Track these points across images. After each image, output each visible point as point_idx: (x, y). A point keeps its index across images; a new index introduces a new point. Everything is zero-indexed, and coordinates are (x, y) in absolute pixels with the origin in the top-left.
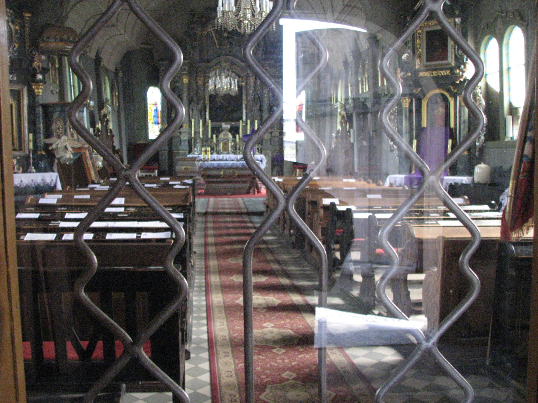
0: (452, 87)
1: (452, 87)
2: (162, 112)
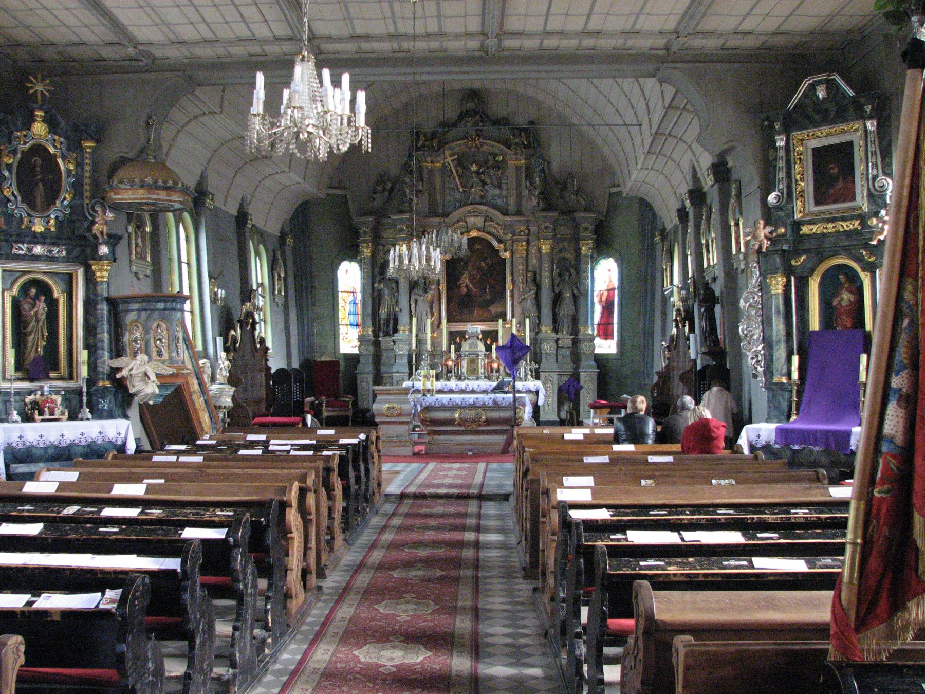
1: (864, 253)
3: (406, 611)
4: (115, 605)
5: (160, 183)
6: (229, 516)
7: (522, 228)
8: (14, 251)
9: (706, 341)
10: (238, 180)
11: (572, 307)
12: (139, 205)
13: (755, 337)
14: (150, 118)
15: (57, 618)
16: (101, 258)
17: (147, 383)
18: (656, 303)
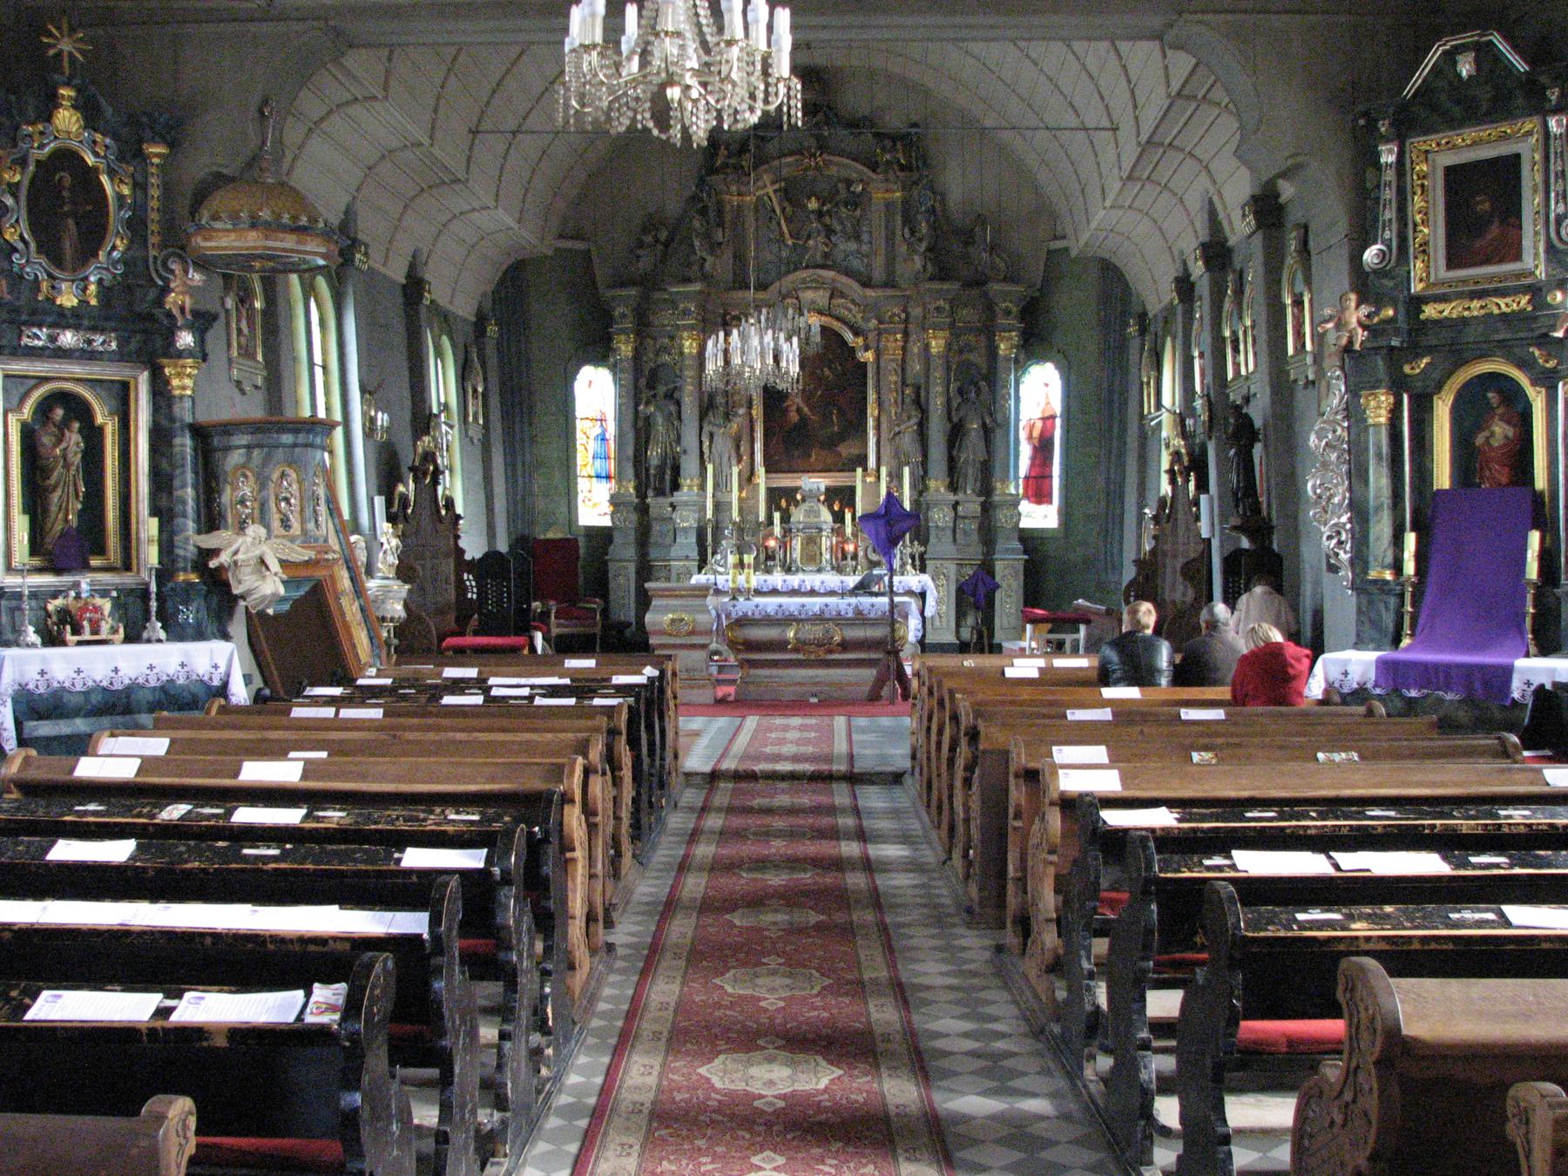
0: (1537, 353)
1: (1537, 353)
2: (620, 437)
3: (772, 990)
4: (337, 1016)
6: (472, 823)
7: (896, 310)
8: (25, 341)
9: (1237, 506)
10: (409, 219)
11: (982, 445)
12: (245, 261)
13: (1336, 500)
14: (266, 102)
15: (221, 1042)
16: (180, 354)
17: (264, 577)
18: (1129, 440)
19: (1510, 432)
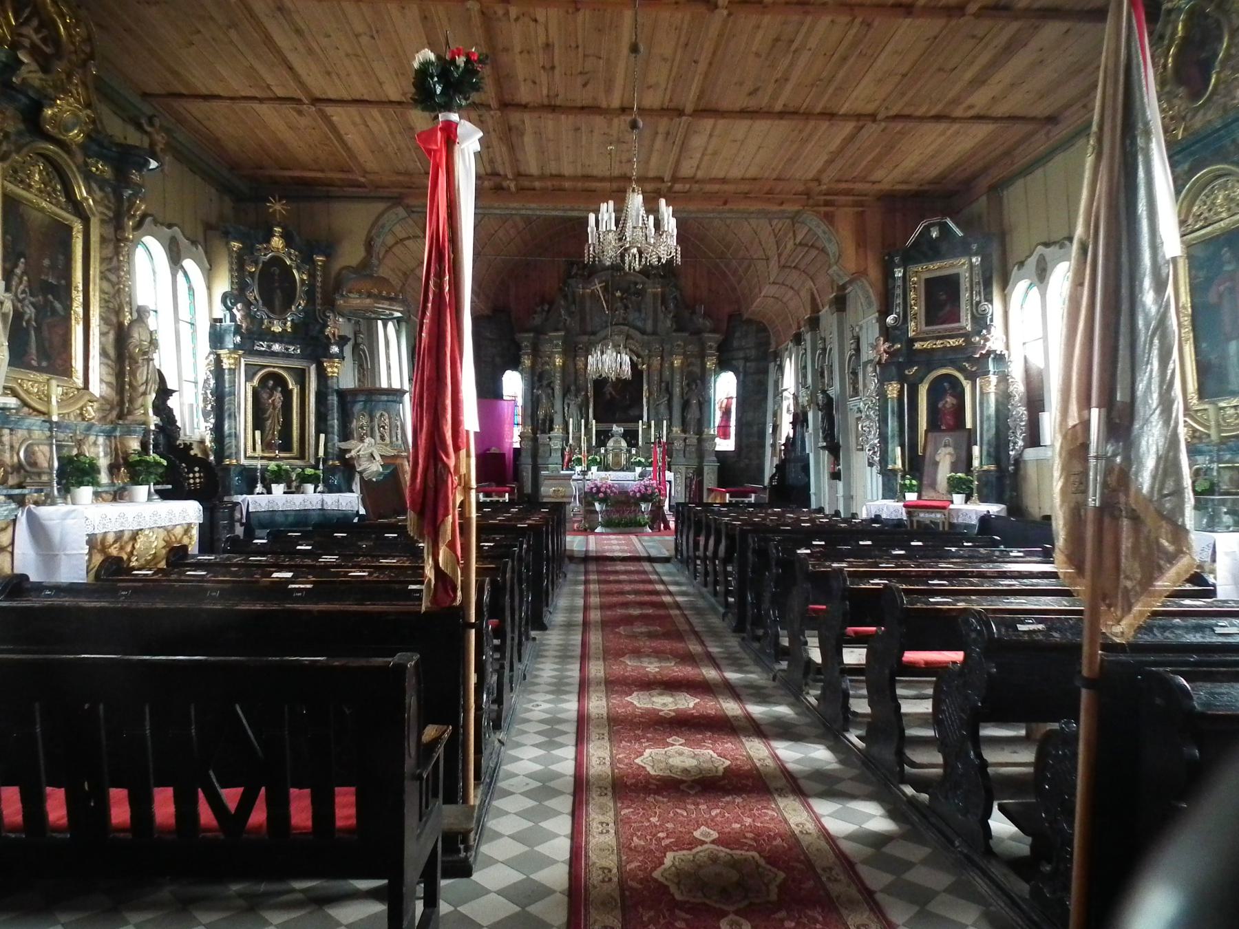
5: (384, 293)
19: (954, 401)
